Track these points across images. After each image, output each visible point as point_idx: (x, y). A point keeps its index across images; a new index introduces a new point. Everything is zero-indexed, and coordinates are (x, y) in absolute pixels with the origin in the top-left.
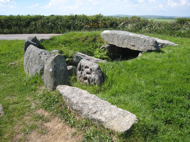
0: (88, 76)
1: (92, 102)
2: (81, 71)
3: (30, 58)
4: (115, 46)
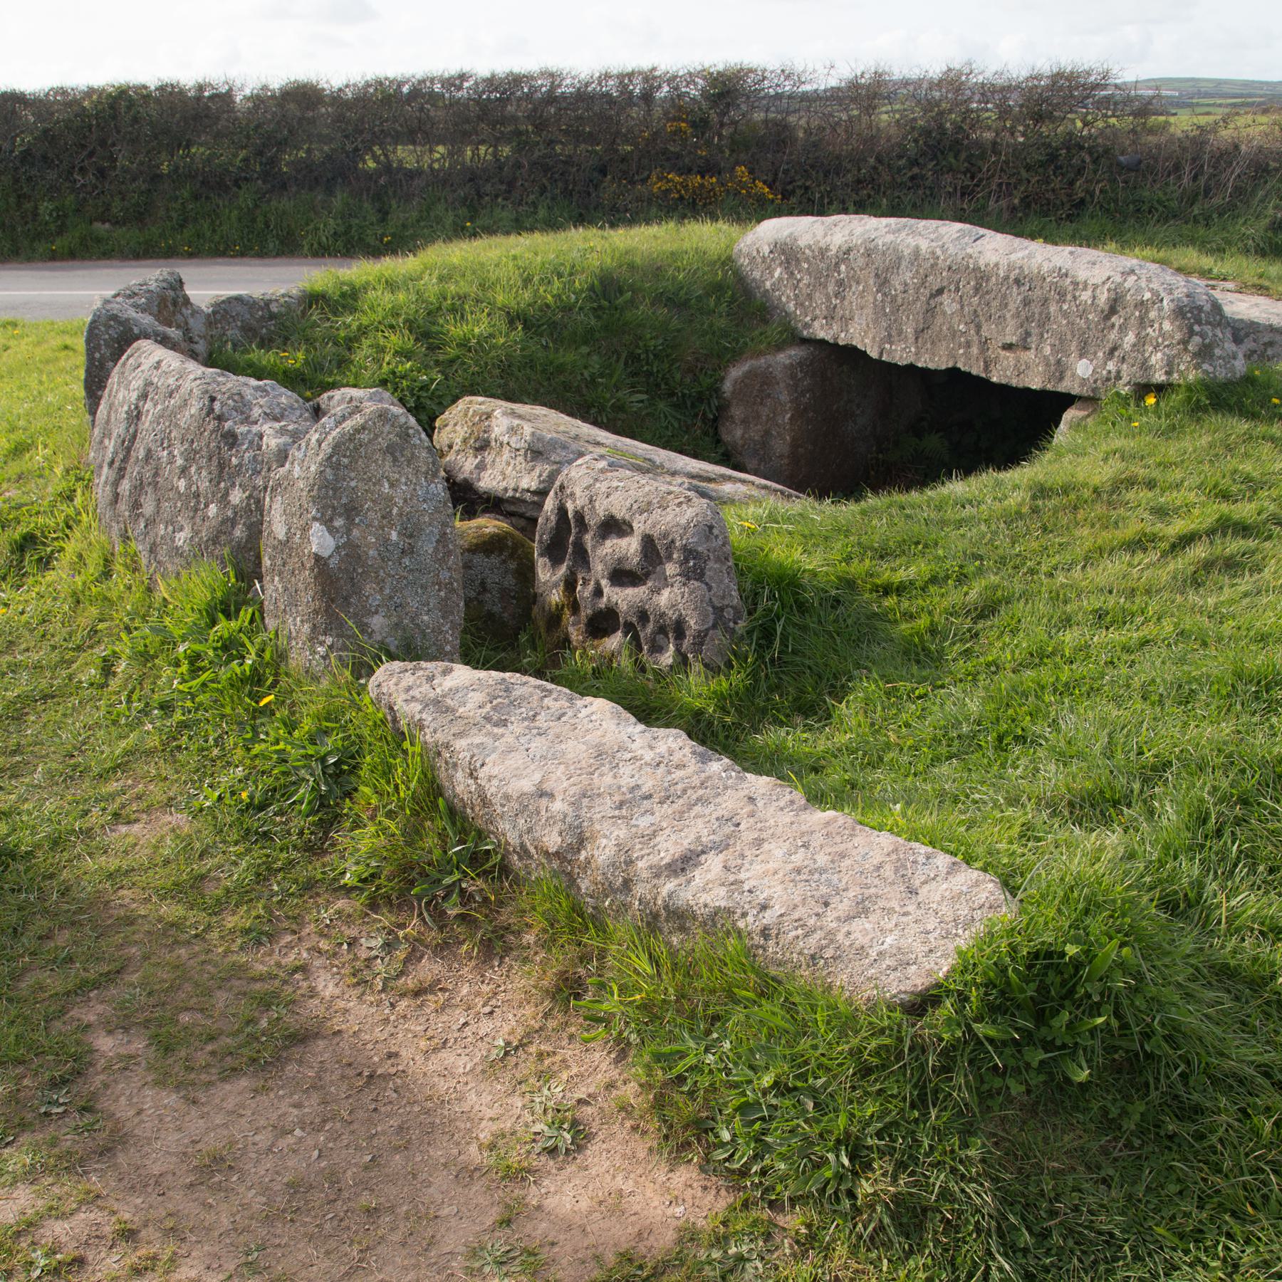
0: (623, 598)
2: (563, 570)
4: (852, 355)
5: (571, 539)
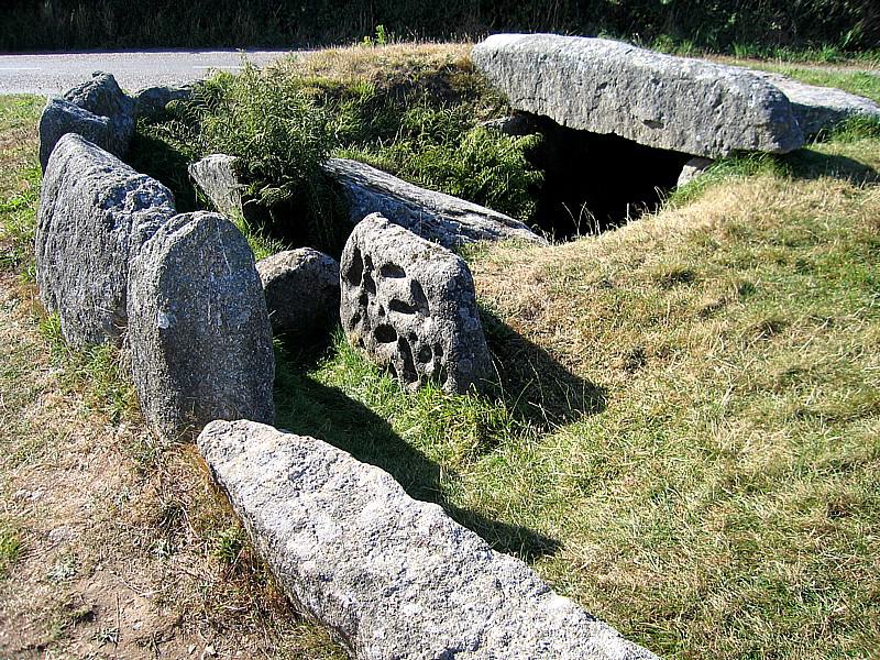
1: (418, 563)
3: (56, 225)
5: (364, 273)
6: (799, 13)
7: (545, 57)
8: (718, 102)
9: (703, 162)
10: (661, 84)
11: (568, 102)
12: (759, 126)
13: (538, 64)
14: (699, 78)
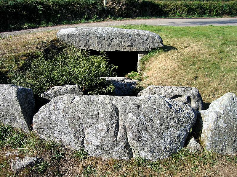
6: (73, 12)
7: (90, 34)
8: (148, 39)
9: (145, 52)
10: (131, 36)
11: (100, 45)
12: (158, 42)
13: (87, 36)
14: (142, 34)
